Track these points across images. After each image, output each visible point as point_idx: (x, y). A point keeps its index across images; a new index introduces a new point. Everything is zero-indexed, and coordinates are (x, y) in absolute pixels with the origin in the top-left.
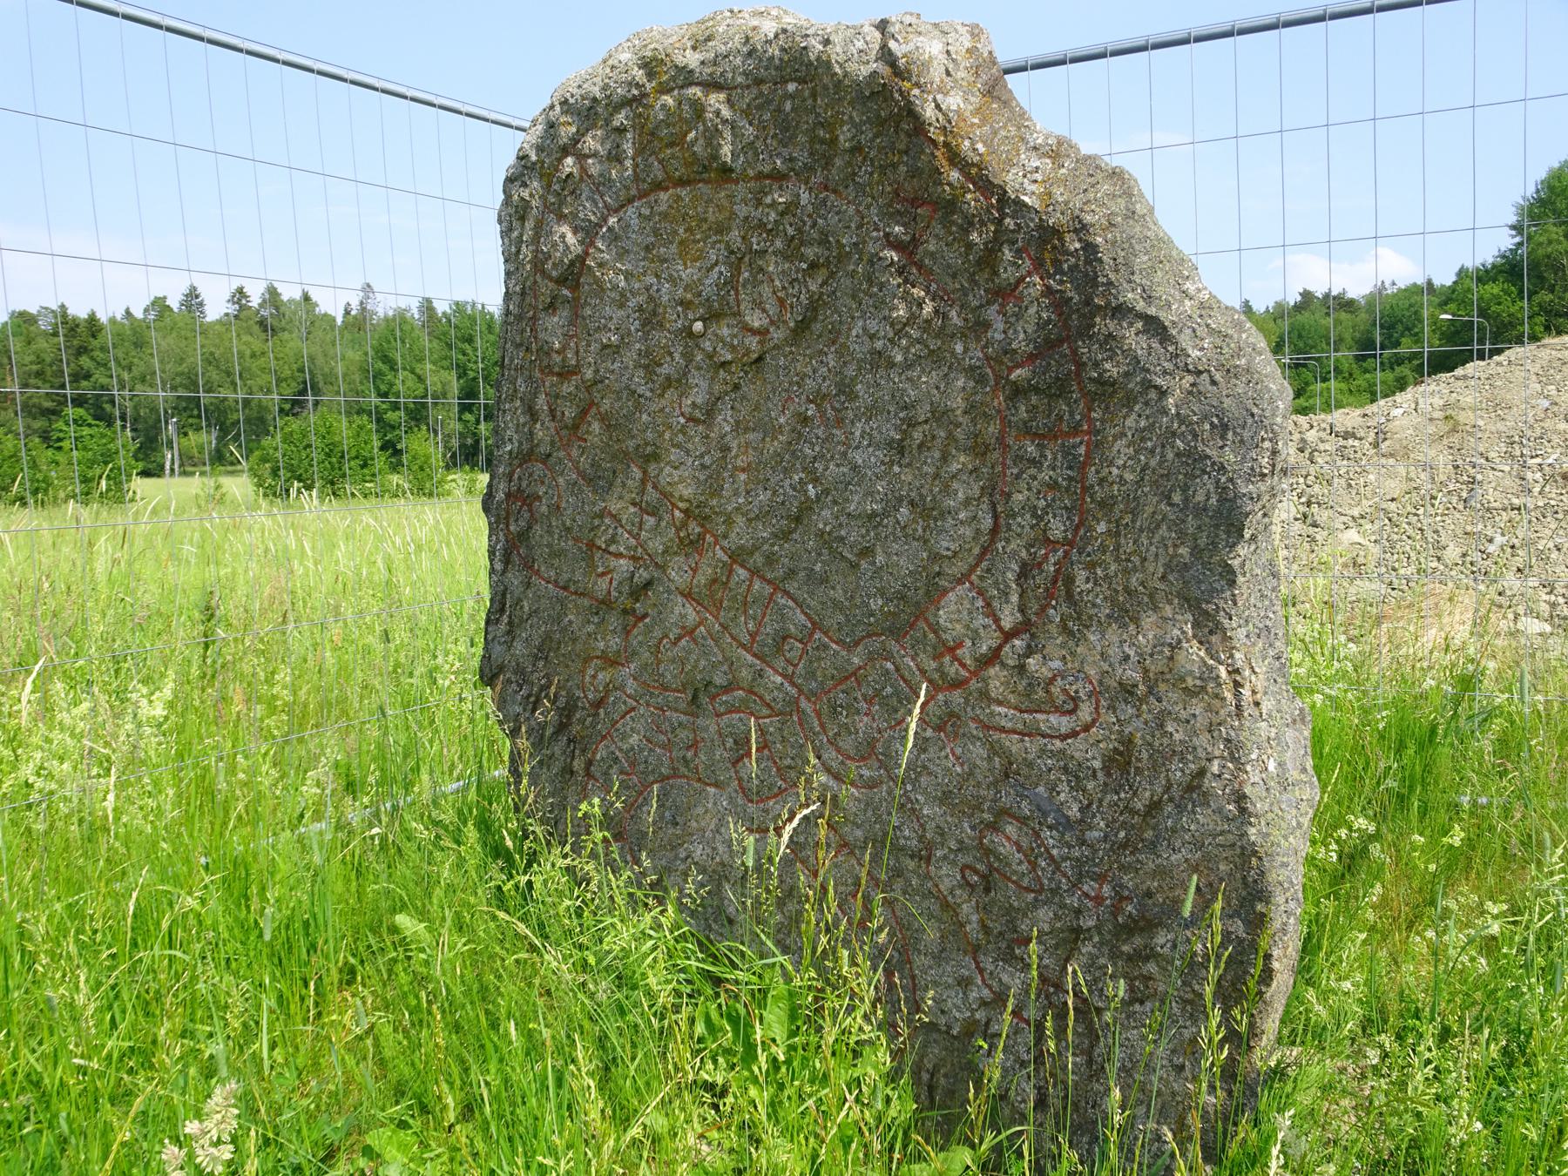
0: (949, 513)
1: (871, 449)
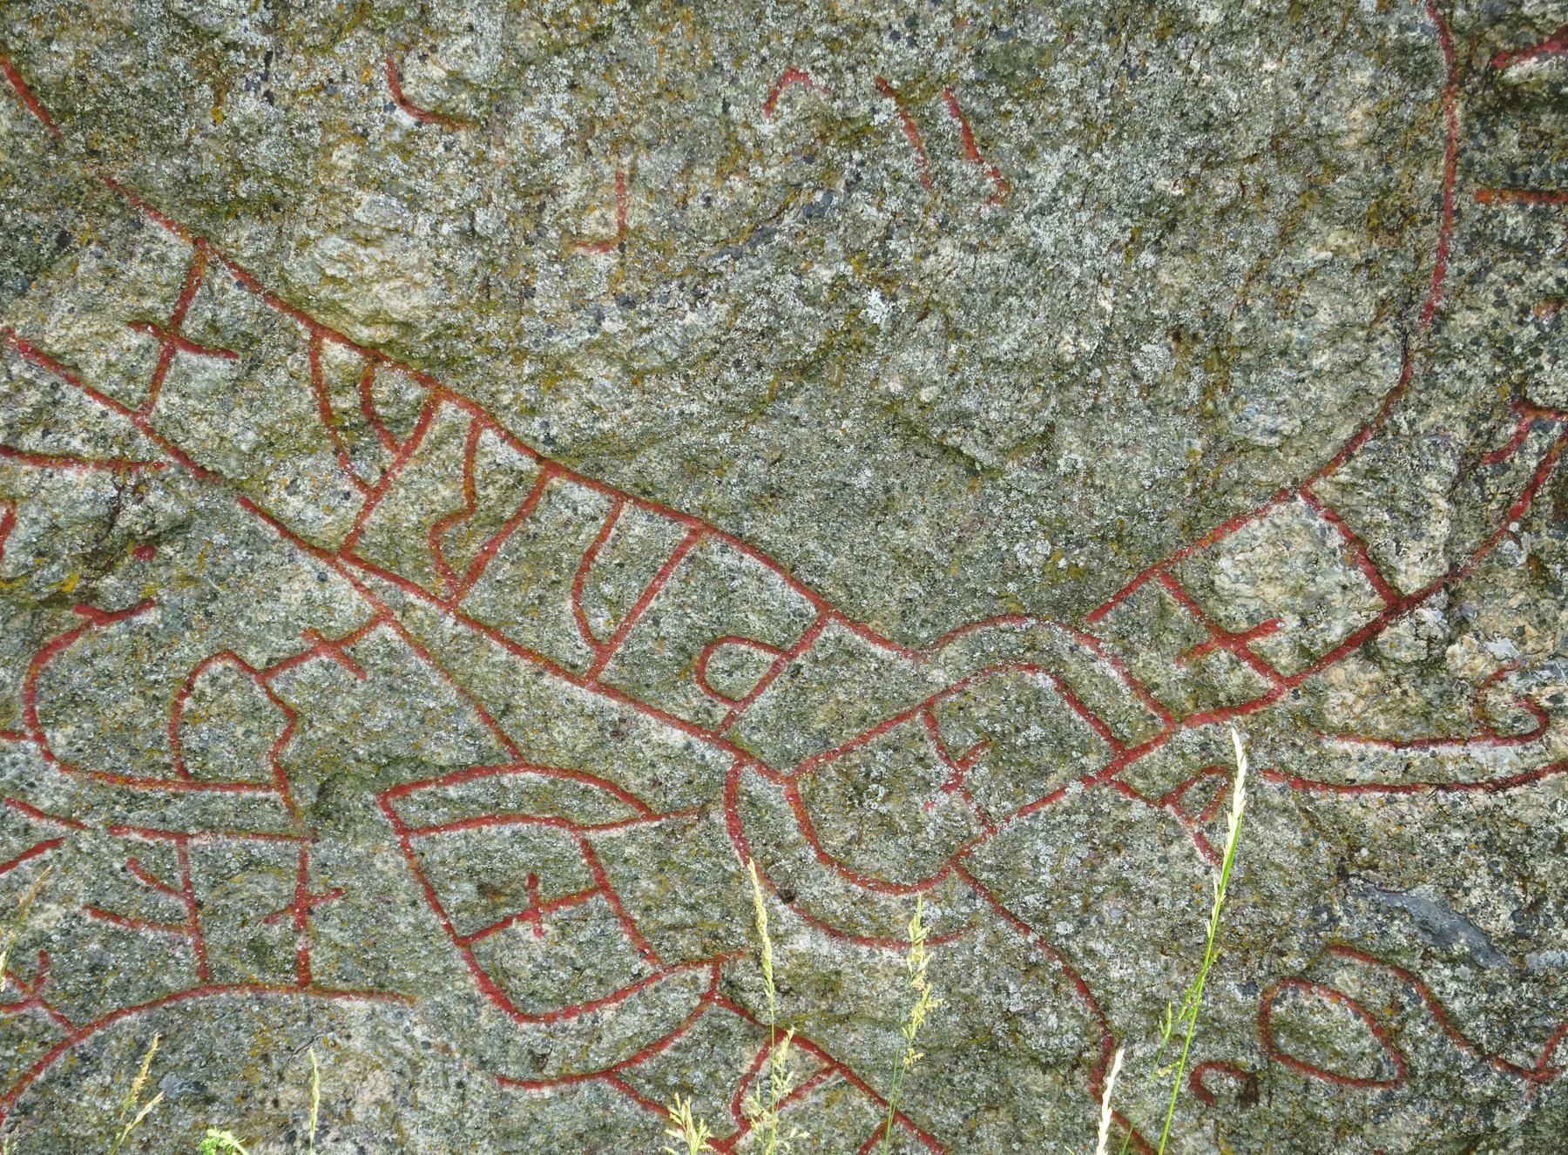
0: (1283, 353)
1: (1084, 216)
